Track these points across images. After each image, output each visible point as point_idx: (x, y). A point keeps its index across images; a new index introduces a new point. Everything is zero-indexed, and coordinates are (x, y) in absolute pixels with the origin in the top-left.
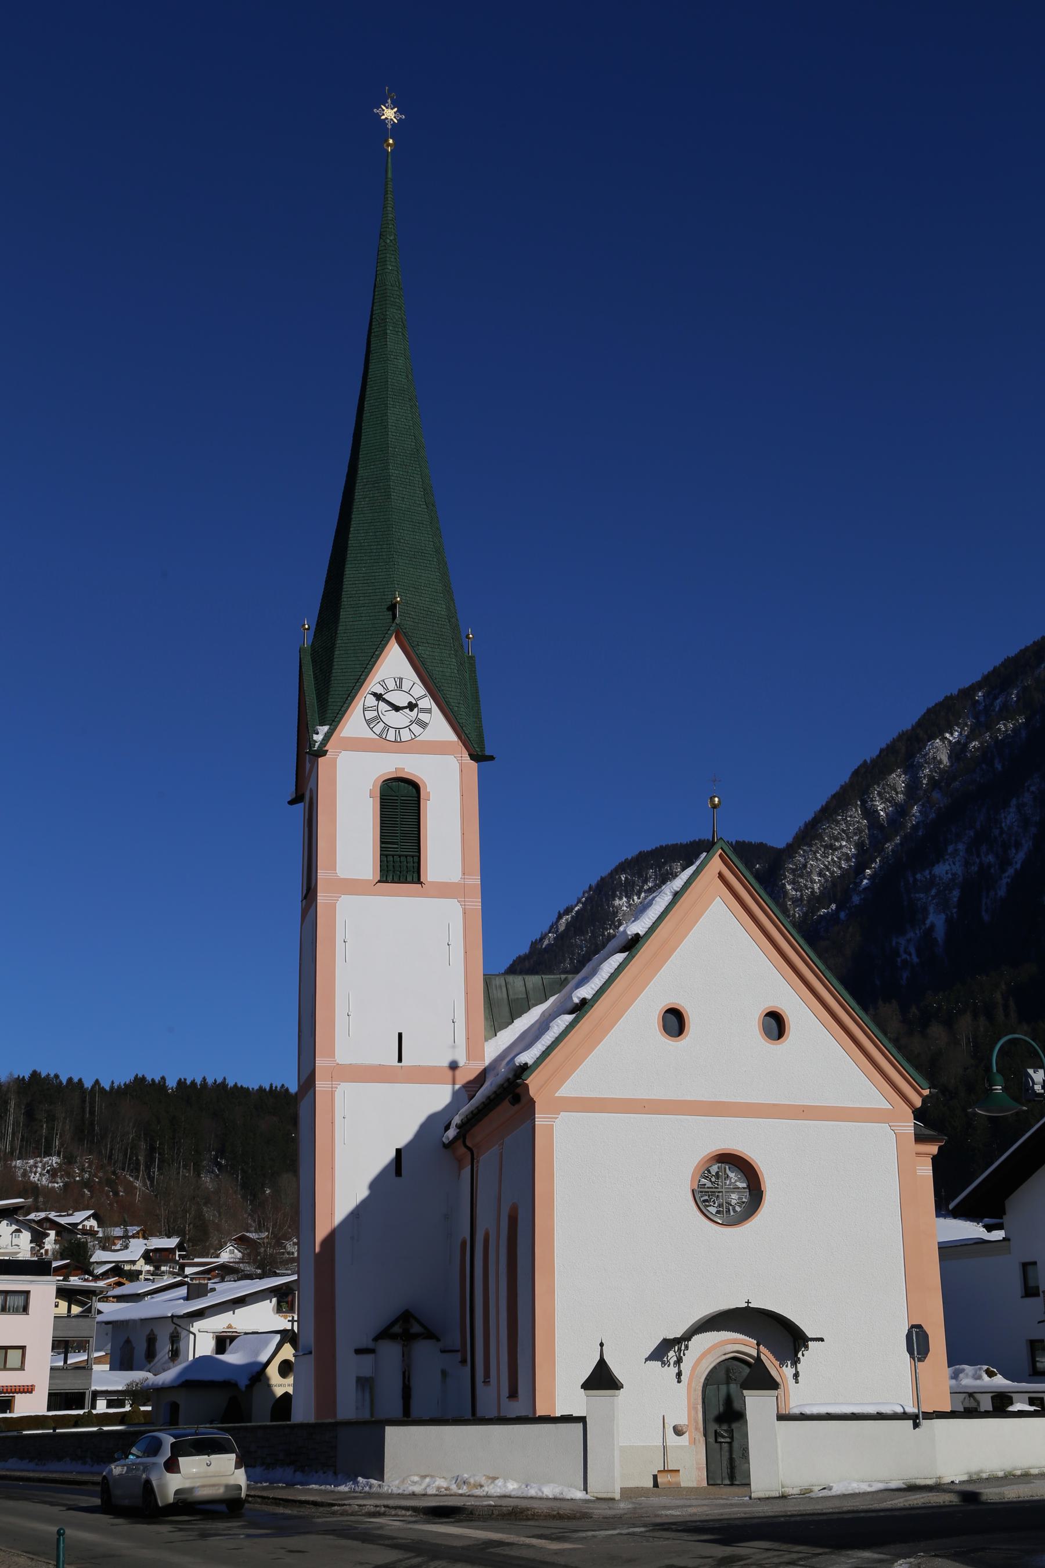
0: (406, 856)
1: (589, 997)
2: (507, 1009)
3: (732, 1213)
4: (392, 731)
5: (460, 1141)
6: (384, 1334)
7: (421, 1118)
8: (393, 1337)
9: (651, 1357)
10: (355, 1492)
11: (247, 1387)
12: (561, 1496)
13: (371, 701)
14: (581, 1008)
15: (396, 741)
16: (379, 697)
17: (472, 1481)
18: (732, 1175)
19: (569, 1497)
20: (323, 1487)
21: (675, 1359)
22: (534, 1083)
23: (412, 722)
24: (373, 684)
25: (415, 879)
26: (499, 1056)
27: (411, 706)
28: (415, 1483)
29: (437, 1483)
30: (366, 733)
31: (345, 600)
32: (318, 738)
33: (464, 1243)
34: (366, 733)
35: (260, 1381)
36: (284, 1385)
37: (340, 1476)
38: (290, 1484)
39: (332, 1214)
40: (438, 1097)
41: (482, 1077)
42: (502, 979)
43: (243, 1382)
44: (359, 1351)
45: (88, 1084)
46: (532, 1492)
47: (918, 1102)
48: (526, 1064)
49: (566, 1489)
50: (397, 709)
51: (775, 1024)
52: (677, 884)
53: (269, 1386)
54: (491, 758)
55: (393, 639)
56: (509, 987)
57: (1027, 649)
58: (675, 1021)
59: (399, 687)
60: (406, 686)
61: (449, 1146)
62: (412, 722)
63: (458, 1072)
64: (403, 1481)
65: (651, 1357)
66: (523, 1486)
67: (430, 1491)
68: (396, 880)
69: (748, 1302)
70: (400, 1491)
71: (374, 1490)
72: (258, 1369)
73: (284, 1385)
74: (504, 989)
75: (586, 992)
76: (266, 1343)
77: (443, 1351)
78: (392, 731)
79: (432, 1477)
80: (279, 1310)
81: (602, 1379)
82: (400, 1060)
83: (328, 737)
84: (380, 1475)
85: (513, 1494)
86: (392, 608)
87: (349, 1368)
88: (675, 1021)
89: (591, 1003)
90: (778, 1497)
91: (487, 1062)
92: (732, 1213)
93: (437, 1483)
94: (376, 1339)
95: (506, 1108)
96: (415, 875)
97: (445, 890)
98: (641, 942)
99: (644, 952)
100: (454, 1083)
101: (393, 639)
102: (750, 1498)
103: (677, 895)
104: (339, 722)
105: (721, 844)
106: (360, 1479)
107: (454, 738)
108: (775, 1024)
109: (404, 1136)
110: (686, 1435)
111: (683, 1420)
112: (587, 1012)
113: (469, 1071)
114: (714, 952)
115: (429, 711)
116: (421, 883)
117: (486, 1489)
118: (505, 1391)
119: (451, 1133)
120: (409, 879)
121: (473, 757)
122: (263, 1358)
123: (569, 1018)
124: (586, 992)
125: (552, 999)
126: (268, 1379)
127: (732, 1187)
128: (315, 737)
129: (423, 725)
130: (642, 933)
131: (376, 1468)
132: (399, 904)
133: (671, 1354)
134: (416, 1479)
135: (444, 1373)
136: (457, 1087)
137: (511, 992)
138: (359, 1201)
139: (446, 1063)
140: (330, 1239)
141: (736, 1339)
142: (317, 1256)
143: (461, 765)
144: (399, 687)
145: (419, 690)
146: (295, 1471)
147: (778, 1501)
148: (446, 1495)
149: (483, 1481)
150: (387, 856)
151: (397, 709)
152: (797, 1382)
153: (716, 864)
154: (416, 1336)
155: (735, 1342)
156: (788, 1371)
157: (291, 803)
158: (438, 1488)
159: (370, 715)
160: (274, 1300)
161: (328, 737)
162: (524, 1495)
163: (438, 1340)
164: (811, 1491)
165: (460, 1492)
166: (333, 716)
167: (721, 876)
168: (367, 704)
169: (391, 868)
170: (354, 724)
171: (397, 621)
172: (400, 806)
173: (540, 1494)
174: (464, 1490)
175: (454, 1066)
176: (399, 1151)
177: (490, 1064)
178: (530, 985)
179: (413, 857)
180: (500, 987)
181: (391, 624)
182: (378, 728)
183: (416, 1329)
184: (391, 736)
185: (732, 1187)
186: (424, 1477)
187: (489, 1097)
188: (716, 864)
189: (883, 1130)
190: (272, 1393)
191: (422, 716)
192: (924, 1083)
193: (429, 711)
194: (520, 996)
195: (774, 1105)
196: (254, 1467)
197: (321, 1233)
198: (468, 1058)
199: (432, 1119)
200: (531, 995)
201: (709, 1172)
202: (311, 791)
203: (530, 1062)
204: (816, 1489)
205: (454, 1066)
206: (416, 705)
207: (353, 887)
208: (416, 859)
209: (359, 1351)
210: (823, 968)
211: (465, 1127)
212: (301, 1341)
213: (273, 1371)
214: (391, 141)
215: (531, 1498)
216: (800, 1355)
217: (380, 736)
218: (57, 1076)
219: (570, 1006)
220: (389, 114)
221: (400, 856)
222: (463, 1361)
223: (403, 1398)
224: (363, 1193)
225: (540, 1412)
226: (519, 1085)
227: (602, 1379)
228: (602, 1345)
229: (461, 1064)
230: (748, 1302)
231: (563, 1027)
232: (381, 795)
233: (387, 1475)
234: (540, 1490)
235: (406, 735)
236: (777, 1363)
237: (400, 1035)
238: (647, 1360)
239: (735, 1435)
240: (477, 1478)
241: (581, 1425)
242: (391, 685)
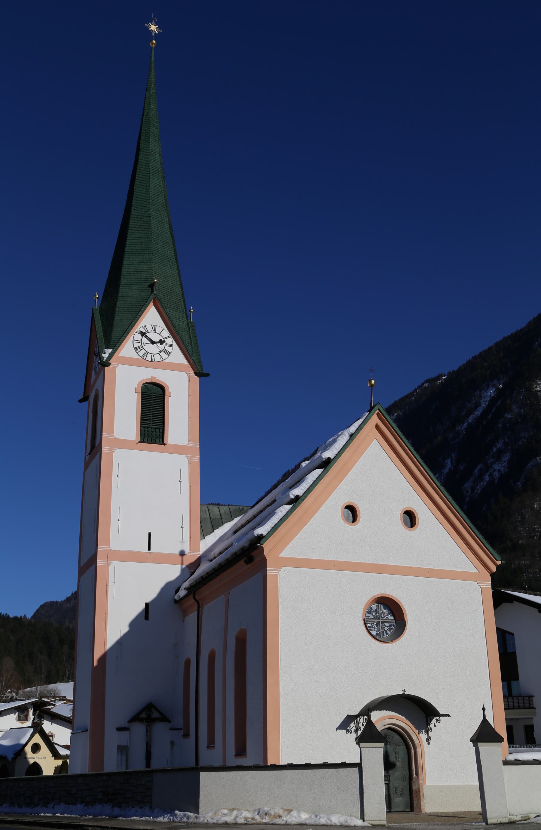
0: (156, 429)
1: (301, 494)
2: (210, 524)
3: (386, 636)
4: (149, 355)
5: (191, 596)
6: (136, 718)
7: (162, 584)
8: (141, 720)
9: (339, 728)
10: (174, 822)
11: (13, 759)
12: (346, 824)
13: (138, 337)
14: (297, 500)
15: (151, 361)
16: (143, 334)
17: (272, 812)
18: (385, 611)
19: (352, 824)
20: (143, 818)
21: (354, 728)
22: (267, 547)
23: (161, 351)
24: (139, 326)
25: (161, 442)
26: (208, 549)
27: (161, 342)
28: (226, 815)
29: (243, 815)
30: (134, 355)
31: (123, 281)
32: (105, 356)
34: (134, 355)
35: (20, 755)
36: (34, 758)
37: (156, 810)
38: (114, 817)
39: (105, 642)
40: (173, 572)
41: (198, 563)
42: (206, 507)
43: (10, 756)
44: (119, 729)
46: (323, 821)
47: (494, 569)
48: (262, 535)
49: (349, 819)
50: (153, 342)
51: (410, 518)
52: (353, 429)
53: (26, 758)
54: (207, 375)
55: (152, 303)
57: (530, 322)
58: (352, 512)
59: (155, 331)
60: (158, 330)
61: (176, 602)
62: (161, 351)
63: (184, 557)
64: (215, 813)
65: (339, 728)
66: (313, 816)
67: (241, 821)
68: (149, 441)
69: (404, 691)
70: (215, 821)
71: (191, 820)
72: (19, 748)
73: (34, 758)
74: (207, 512)
75: (298, 491)
76: (25, 734)
77: (171, 729)
78: (149, 355)
79: (239, 810)
80: (19, 719)
82: (149, 549)
83: (111, 356)
84: (196, 809)
85: (308, 822)
86: (152, 286)
87: (112, 740)
88: (352, 512)
89: (302, 498)
90: (506, 823)
91: (201, 553)
92: (386, 636)
93: (243, 815)
94: (131, 721)
95: (250, 560)
96: (161, 440)
97: (178, 450)
98: (332, 463)
99: (334, 469)
100: (182, 564)
101: (152, 303)
102: (487, 824)
103: (352, 436)
104: (119, 347)
105: (378, 406)
106: (176, 812)
107: (185, 362)
108: (410, 518)
109: (151, 595)
112: (300, 504)
113: (191, 557)
114: (373, 472)
115: (171, 346)
116: (165, 444)
117: (284, 819)
119: (182, 593)
120: (157, 441)
121: (196, 374)
122: (23, 741)
123: (288, 507)
124: (298, 491)
125: (236, 520)
126: (25, 754)
127: (388, 618)
128: (103, 355)
129: (168, 353)
130: (332, 457)
131: (192, 802)
132: (151, 456)
133: (352, 725)
134: (226, 811)
135: (172, 743)
136: (184, 566)
137: (211, 514)
138: (122, 634)
139: (177, 552)
140: (103, 658)
141: (392, 716)
142: (94, 669)
143: (189, 378)
144: (155, 331)
145: (166, 333)
146: (112, 807)
147: (507, 825)
148: (253, 824)
149: (281, 812)
150: (144, 427)
151: (153, 342)
152: (429, 744)
153: (375, 419)
154: (155, 720)
155: (391, 717)
156: (423, 737)
157: (81, 401)
158: (246, 819)
159: (137, 345)
160: (17, 714)
161: (111, 356)
162: (317, 823)
163: (170, 722)
164: (529, 819)
165: (264, 821)
166: (115, 344)
167: (377, 427)
168: (135, 339)
169: (146, 435)
170: (127, 349)
171: (155, 292)
172: (153, 398)
173: (329, 823)
174: (266, 820)
175: (182, 554)
176: (147, 604)
177: (203, 554)
178: (222, 511)
179: (160, 429)
180: (205, 511)
181: (150, 294)
182: (142, 353)
183: (155, 715)
184: (149, 358)
185: (388, 618)
186: (232, 810)
187: (220, 564)
188: (375, 419)
190: (28, 762)
191: (167, 348)
192: (498, 557)
193: (171, 346)
194: (217, 517)
195: (411, 567)
196: (75, 804)
197: (98, 654)
198: (190, 549)
199: (168, 585)
200: (223, 517)
201: (371, 608)
202: (97, 391)
203: (265, 533)
204: (532, 816)
205: (182, 554)
206: (164, 342)
207: (124, 444)
208: (161, 430)
209: (119, 729)
210: (439, 484)
211: (192, 590)
212: (76, 723)
213: (28, 749)
214: (154, 42)
215: (323, 825)
216: (432, 726)
217: (142, 357)
219: (287, 500)
220: (153, 28)
221: (152, 428)
224: (125, 629)
225: (270, 762)
226: (258, 547)
229: (186, 553)
230: (404, 691)
231: (284, 512)
232: (142, 392)
233: (201, 810)
234: (329, 819)
235: (157, 358)
236: (417, 731)
237: (150, 534)
238: (337, 729)
239: (391, 779)
240: (276, 811)
241: (357, 770)
242: (150, 329)
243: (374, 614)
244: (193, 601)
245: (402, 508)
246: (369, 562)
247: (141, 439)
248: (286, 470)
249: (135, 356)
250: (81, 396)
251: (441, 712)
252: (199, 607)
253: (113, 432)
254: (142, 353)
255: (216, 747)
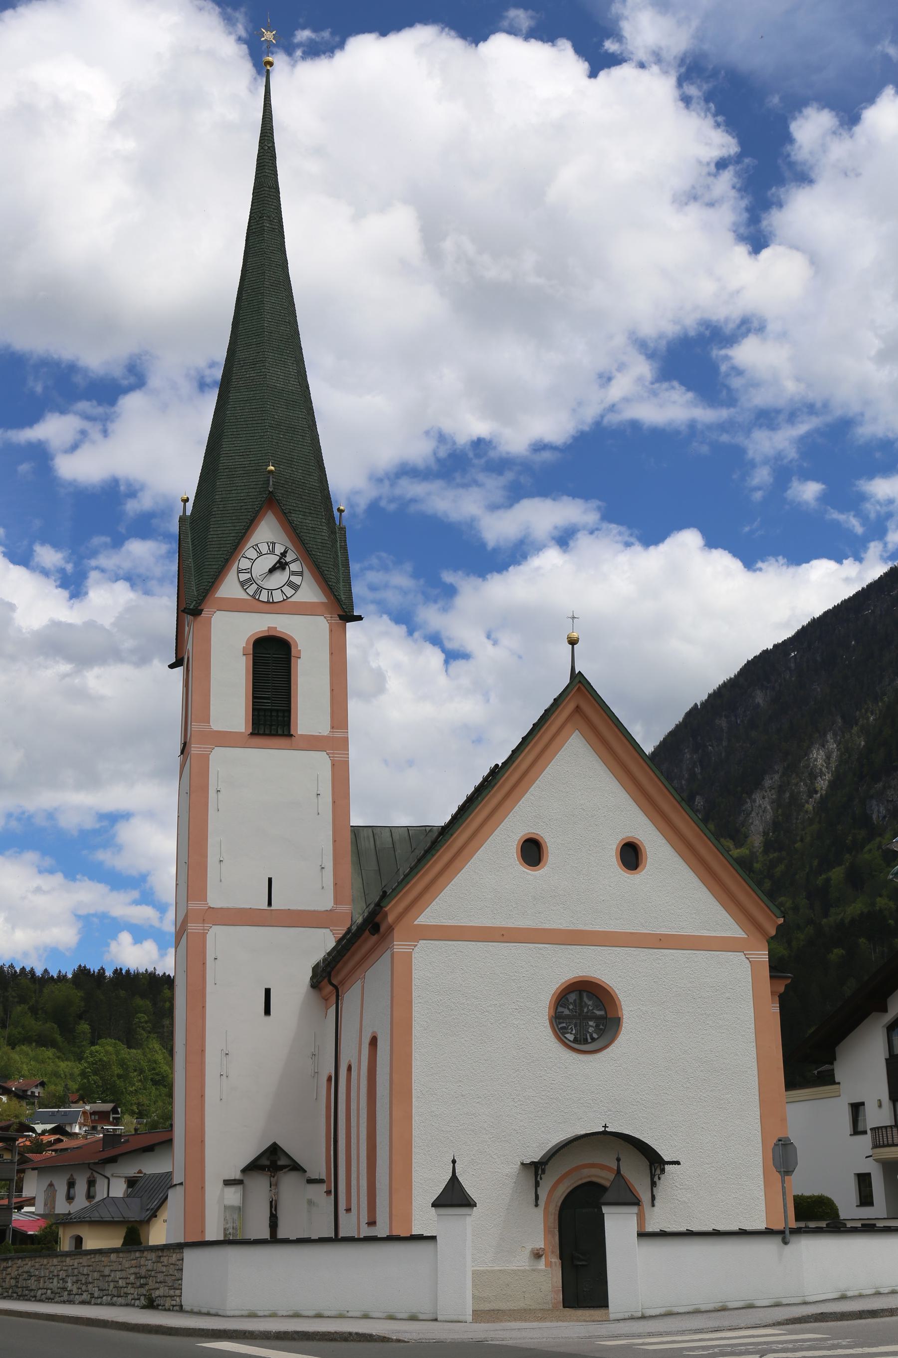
0: (277, 711)
6: (253, 1167)
15: (268, 602)
18: (590, 1003)
30: (239, 594)
33: (329, 1079)
34: (239, 594)
44: (228, 1183)
45: (39, 972)
51: (631, 855)
56: (377, 837)
58: (532, 851)
68: (267, 732)
69: (605, 1127)
77: (310, 1181)
78: (264, 592)
81: (454, 1197)
82: (270, 904)
88: (532, 851)
94: (245, 1171)
97: (314, 743)
108: (631, 855)
110: (543, 1258)
111: (540, 1244)
118: (364, 1219)
127: (586, 1015)
129: (296, 587)
132: (269, 758)
137: (378, 843)
154: (282, 1168)
157: (172, 666)
159: (244, 577)
168: (242, 566)
182: (252, 589)
183: (282, 1162)
184: (264, 597)
185: (586, 1015)
189: (738, 959)
193: (300, 574)
207: (226, 739)
209: (228, 1183)
217: (253, 596)
218: (12, 966)
222: (328, 1192)
223: (270, 1226)
227: (454, 1197)
228: (454, 1162)
230: (605, 1127)
237: (270, 880)
243: (571, 1007)
244: (330, 988)
245: (620, 838)
246: (561, 927)
247: (253, 729)
248: (691, 705)
249: (243, 596)
250: (173, 660)
251: (666, 1159)
252: (337, 996)
253: (208, 721)
254: (252, 589)
255: (776, 1139)
